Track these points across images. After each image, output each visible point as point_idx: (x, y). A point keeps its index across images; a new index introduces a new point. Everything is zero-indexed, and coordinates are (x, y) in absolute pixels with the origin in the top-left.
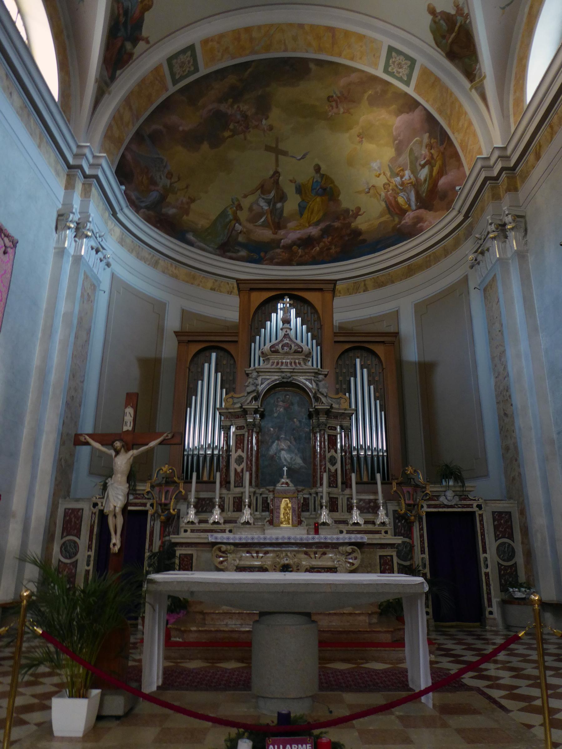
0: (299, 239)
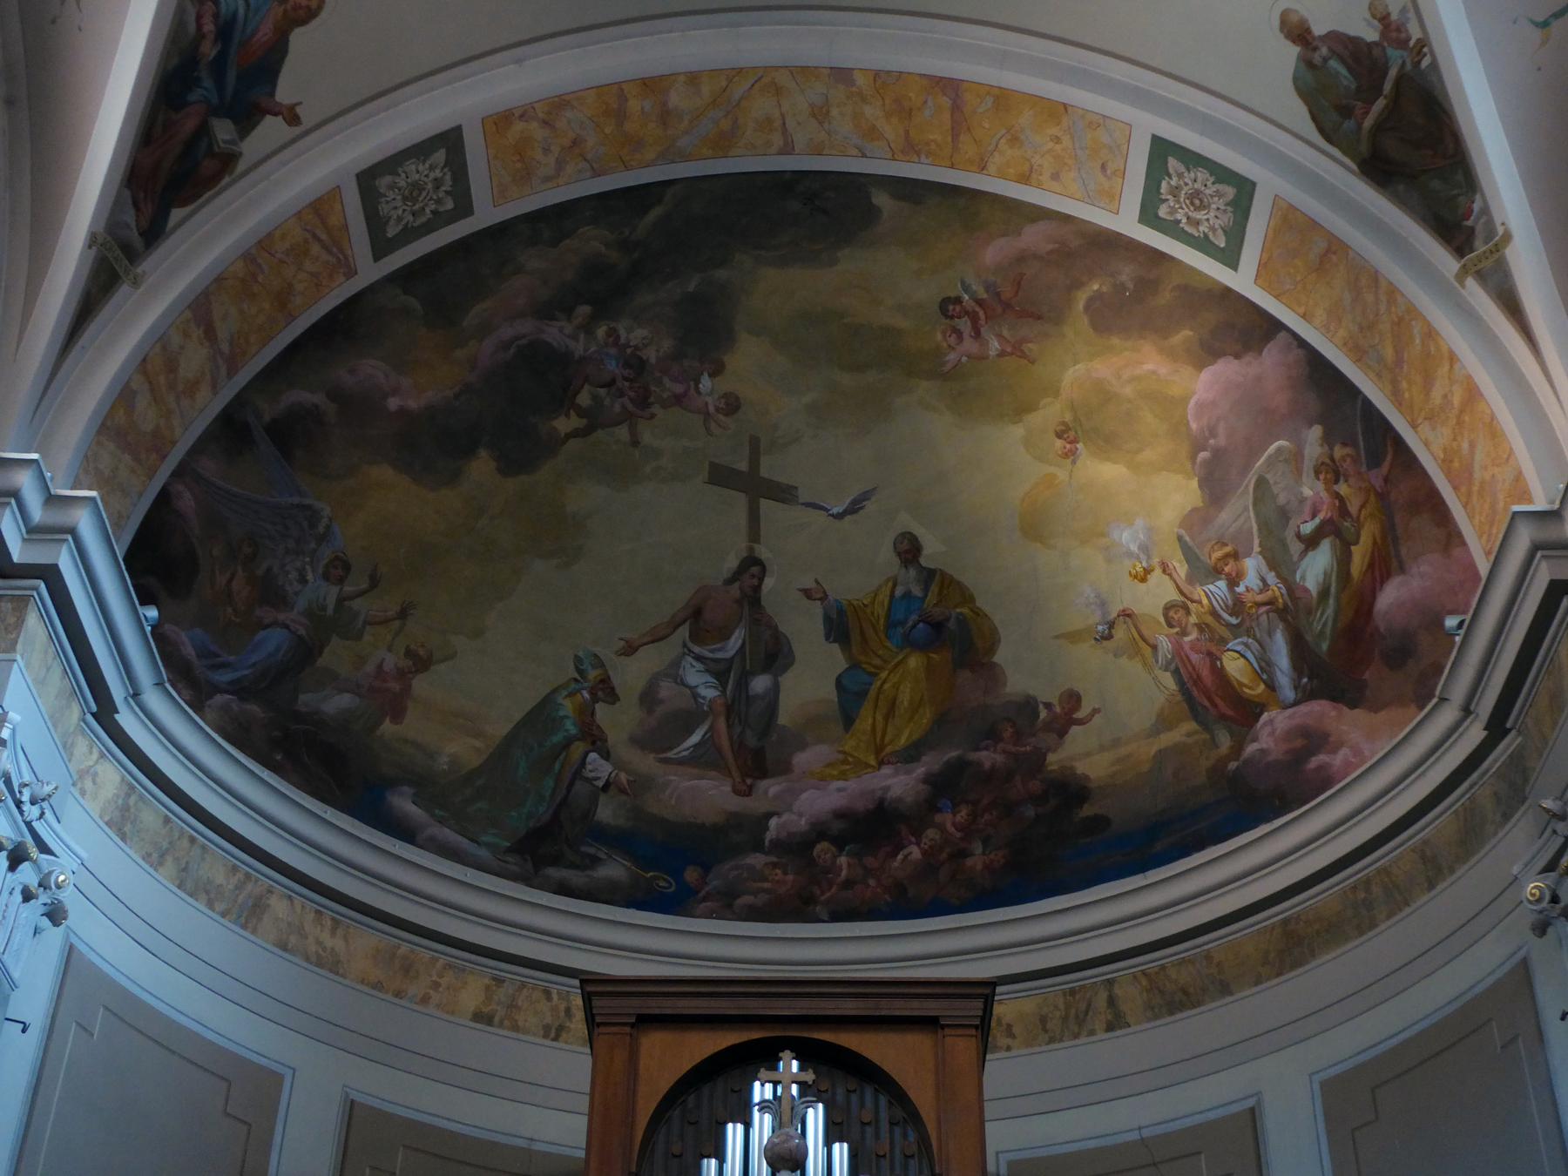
0: (840, 815)
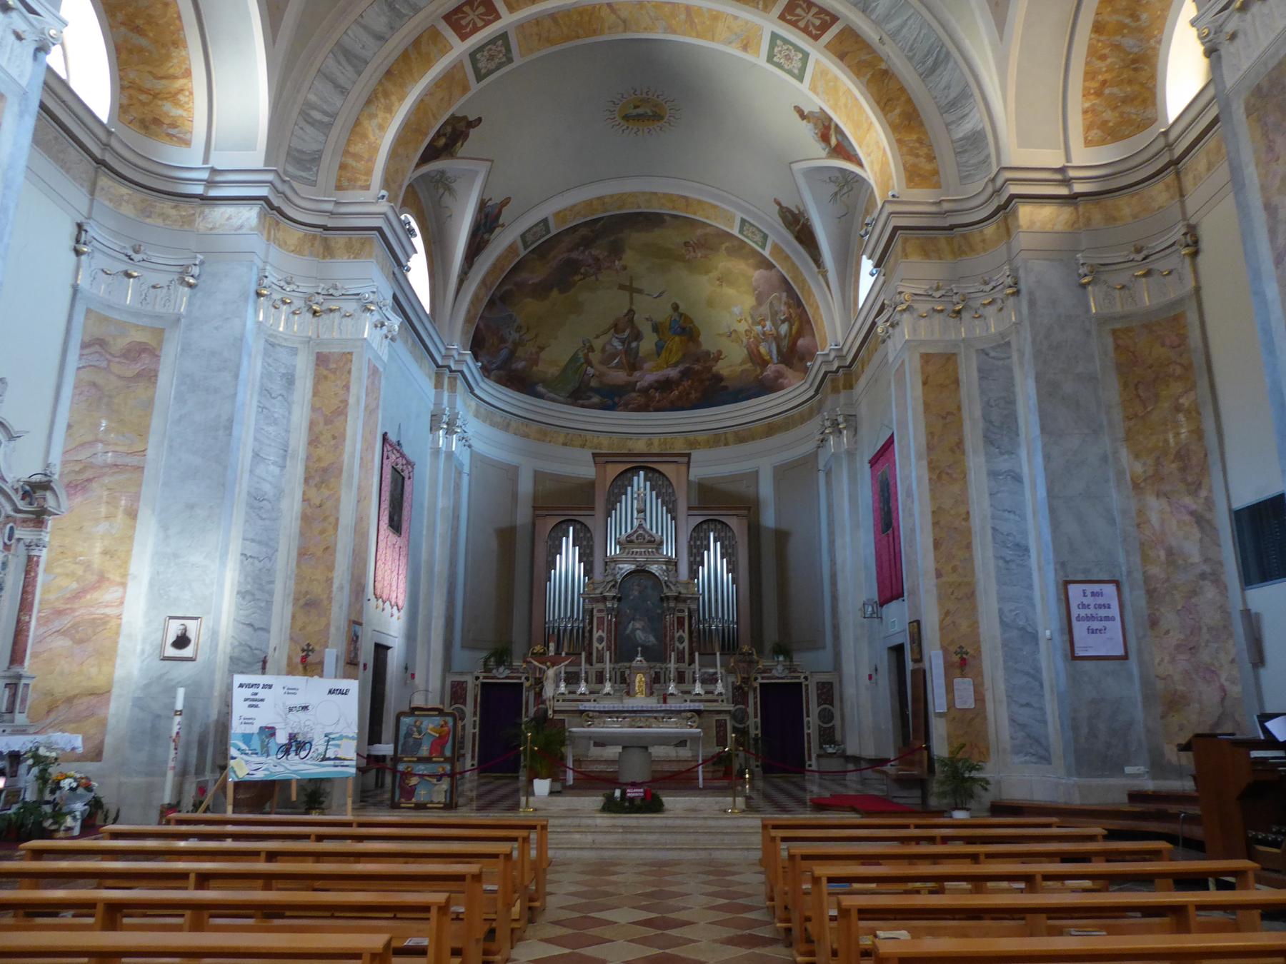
0: (657, 382)
